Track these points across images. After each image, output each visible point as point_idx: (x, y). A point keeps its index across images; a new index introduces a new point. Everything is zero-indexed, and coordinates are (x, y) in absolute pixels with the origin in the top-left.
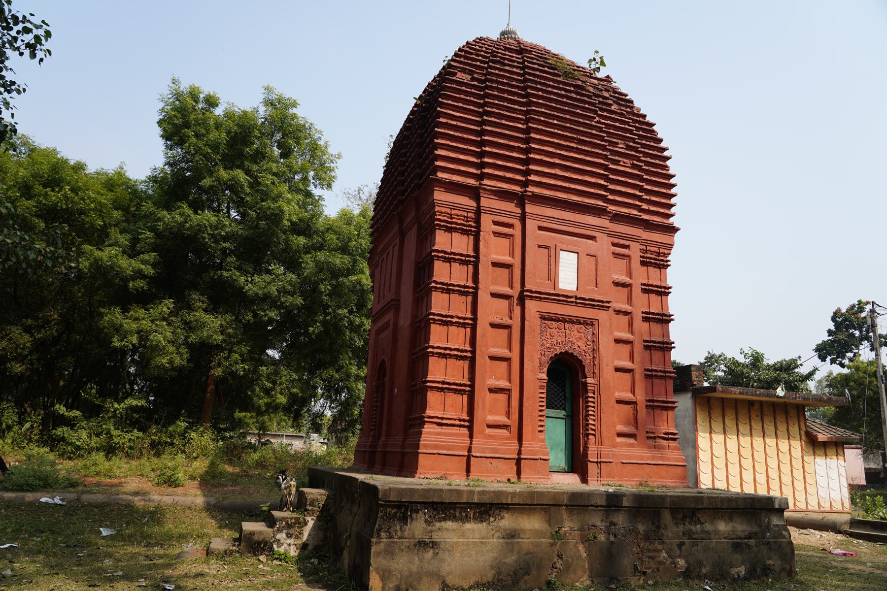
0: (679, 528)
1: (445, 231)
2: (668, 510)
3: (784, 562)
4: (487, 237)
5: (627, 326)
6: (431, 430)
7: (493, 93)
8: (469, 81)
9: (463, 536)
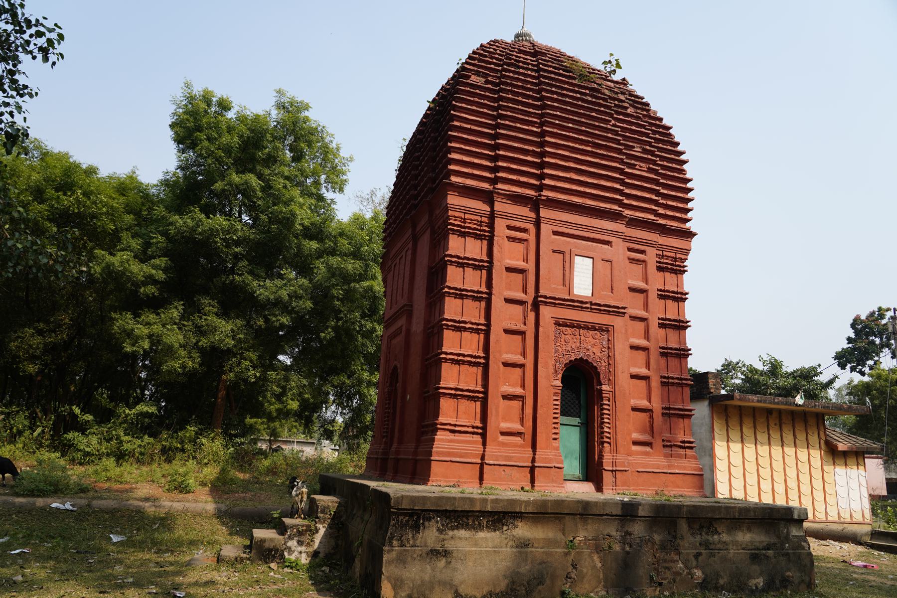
0: (695, 538)
1: (459, 235)
2: (684, 520)
3: (803, 574)
6: (444, 437)
7: (507, 96)
9: (476, 544)
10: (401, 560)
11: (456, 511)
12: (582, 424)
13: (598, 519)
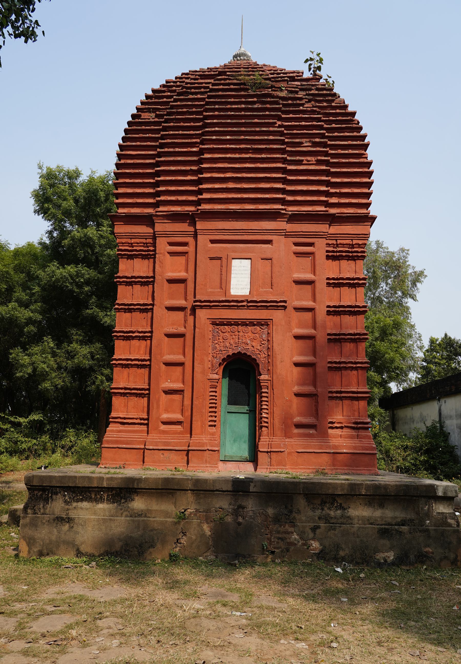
0: (315, 512)
7: (169, 124)
8: (153, 119)
10: (33, 524)
12: (250, 411)
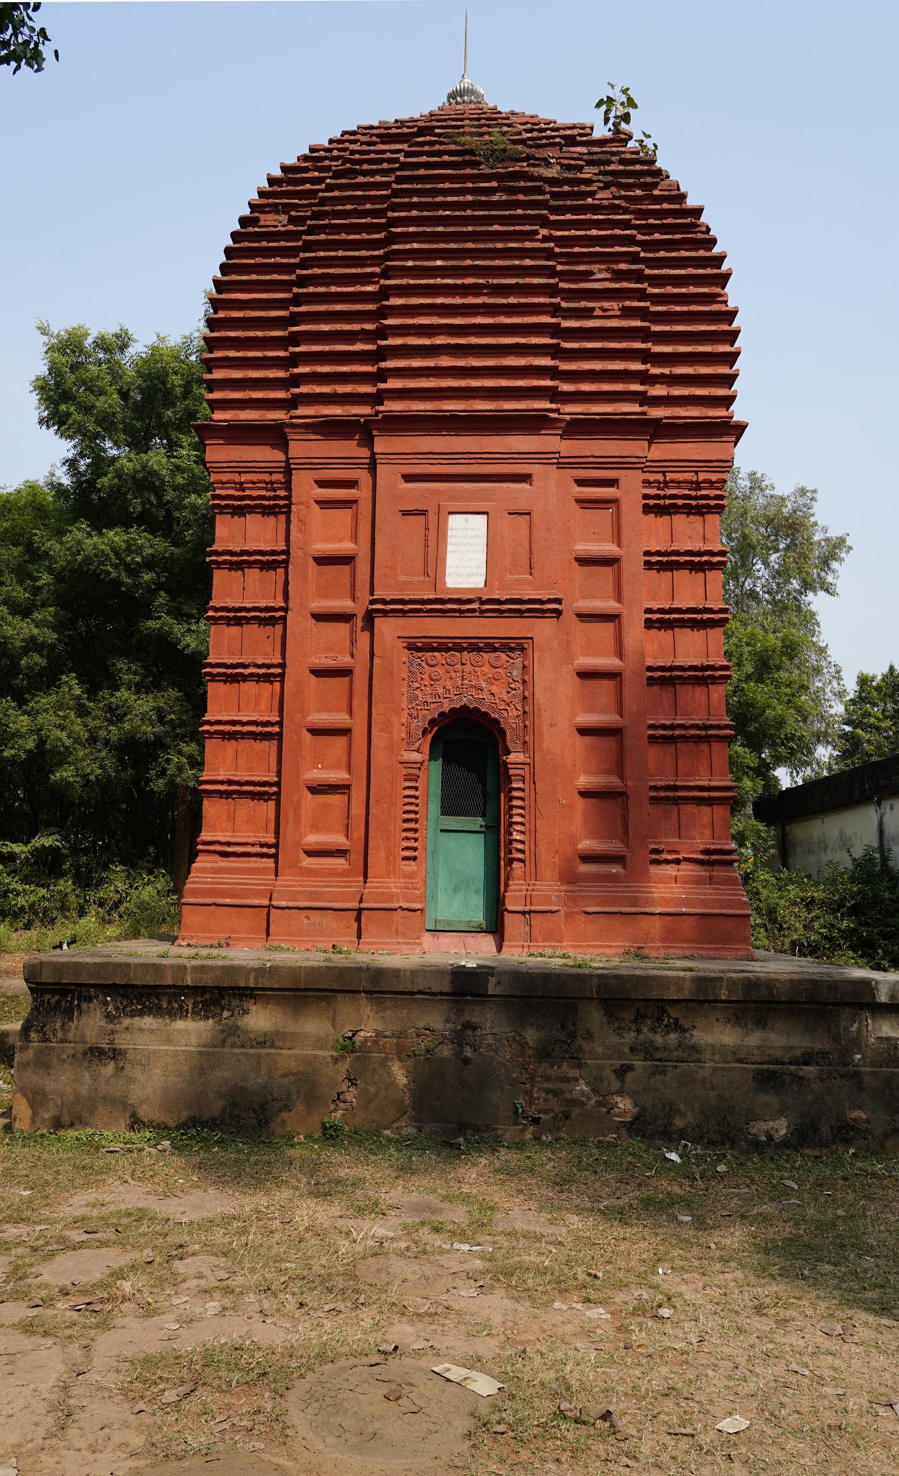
0: (623, 1037)
2: (597, 1002)
4: (304, 512)
5: (611, 643)
6: (208, 865)
7: (317, 237)
8: (284, 226)
9: (169, 1041)
10: (42, 1063)
11: (134, 987)
13: (407, 999)
